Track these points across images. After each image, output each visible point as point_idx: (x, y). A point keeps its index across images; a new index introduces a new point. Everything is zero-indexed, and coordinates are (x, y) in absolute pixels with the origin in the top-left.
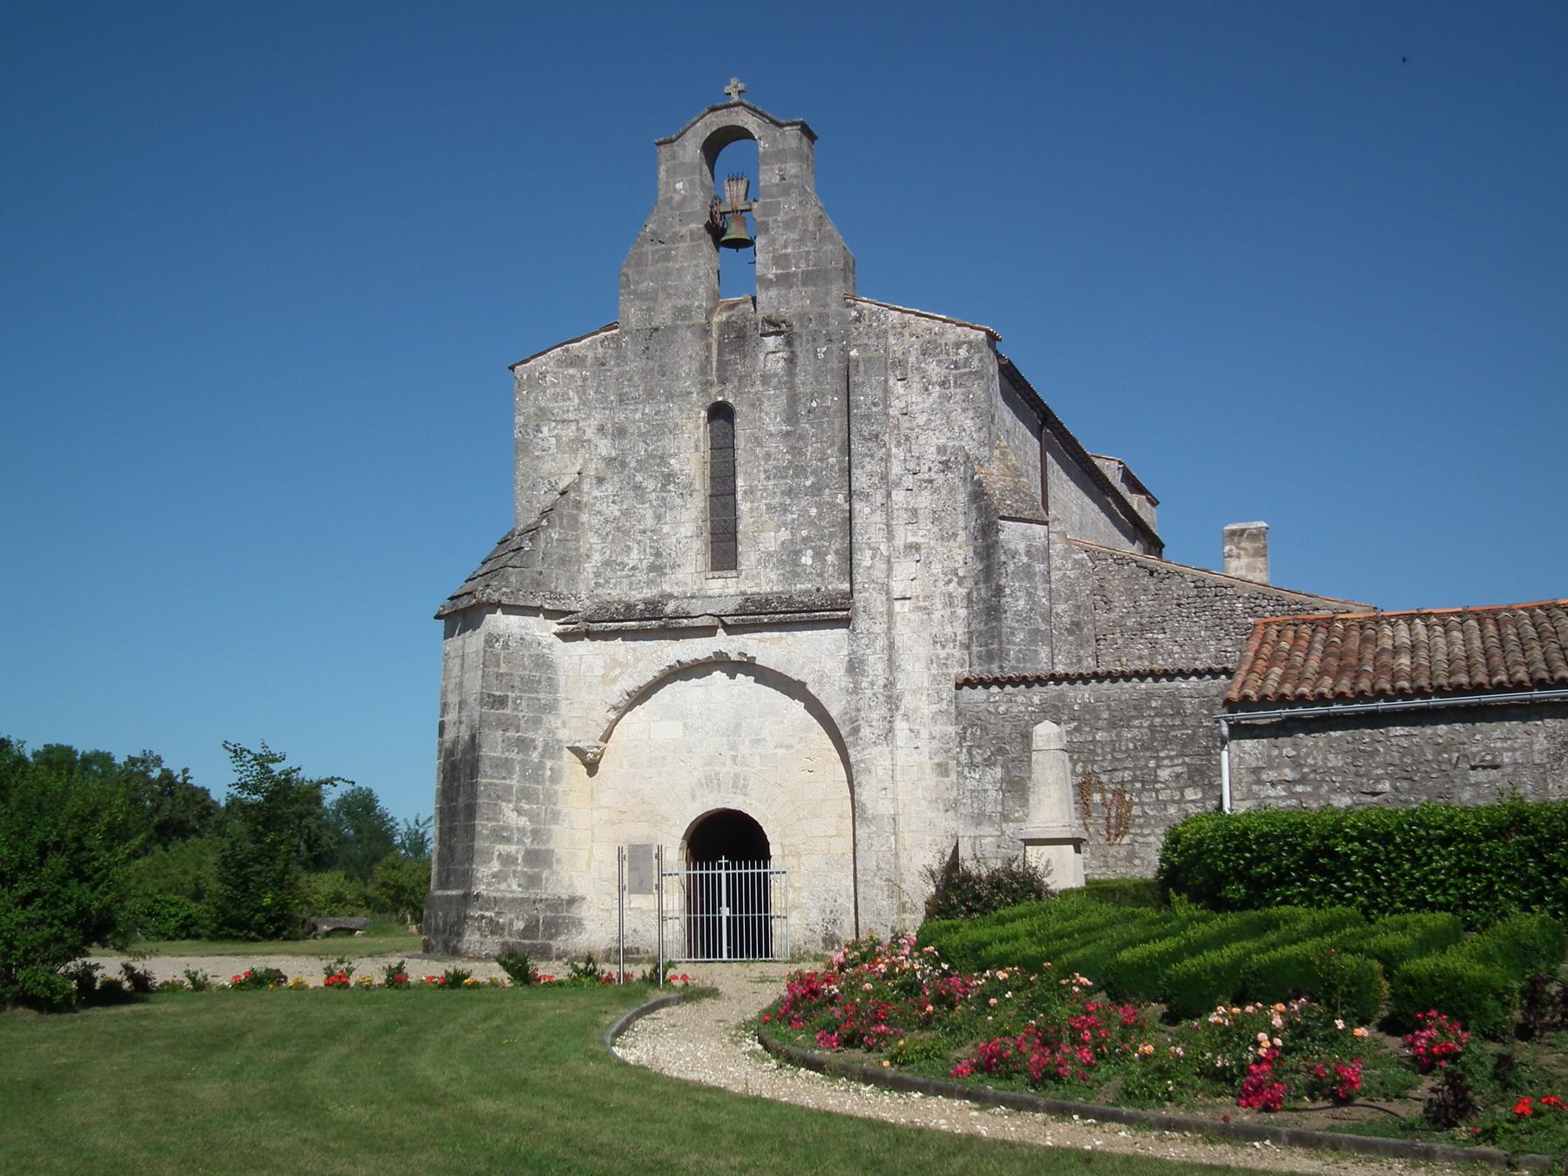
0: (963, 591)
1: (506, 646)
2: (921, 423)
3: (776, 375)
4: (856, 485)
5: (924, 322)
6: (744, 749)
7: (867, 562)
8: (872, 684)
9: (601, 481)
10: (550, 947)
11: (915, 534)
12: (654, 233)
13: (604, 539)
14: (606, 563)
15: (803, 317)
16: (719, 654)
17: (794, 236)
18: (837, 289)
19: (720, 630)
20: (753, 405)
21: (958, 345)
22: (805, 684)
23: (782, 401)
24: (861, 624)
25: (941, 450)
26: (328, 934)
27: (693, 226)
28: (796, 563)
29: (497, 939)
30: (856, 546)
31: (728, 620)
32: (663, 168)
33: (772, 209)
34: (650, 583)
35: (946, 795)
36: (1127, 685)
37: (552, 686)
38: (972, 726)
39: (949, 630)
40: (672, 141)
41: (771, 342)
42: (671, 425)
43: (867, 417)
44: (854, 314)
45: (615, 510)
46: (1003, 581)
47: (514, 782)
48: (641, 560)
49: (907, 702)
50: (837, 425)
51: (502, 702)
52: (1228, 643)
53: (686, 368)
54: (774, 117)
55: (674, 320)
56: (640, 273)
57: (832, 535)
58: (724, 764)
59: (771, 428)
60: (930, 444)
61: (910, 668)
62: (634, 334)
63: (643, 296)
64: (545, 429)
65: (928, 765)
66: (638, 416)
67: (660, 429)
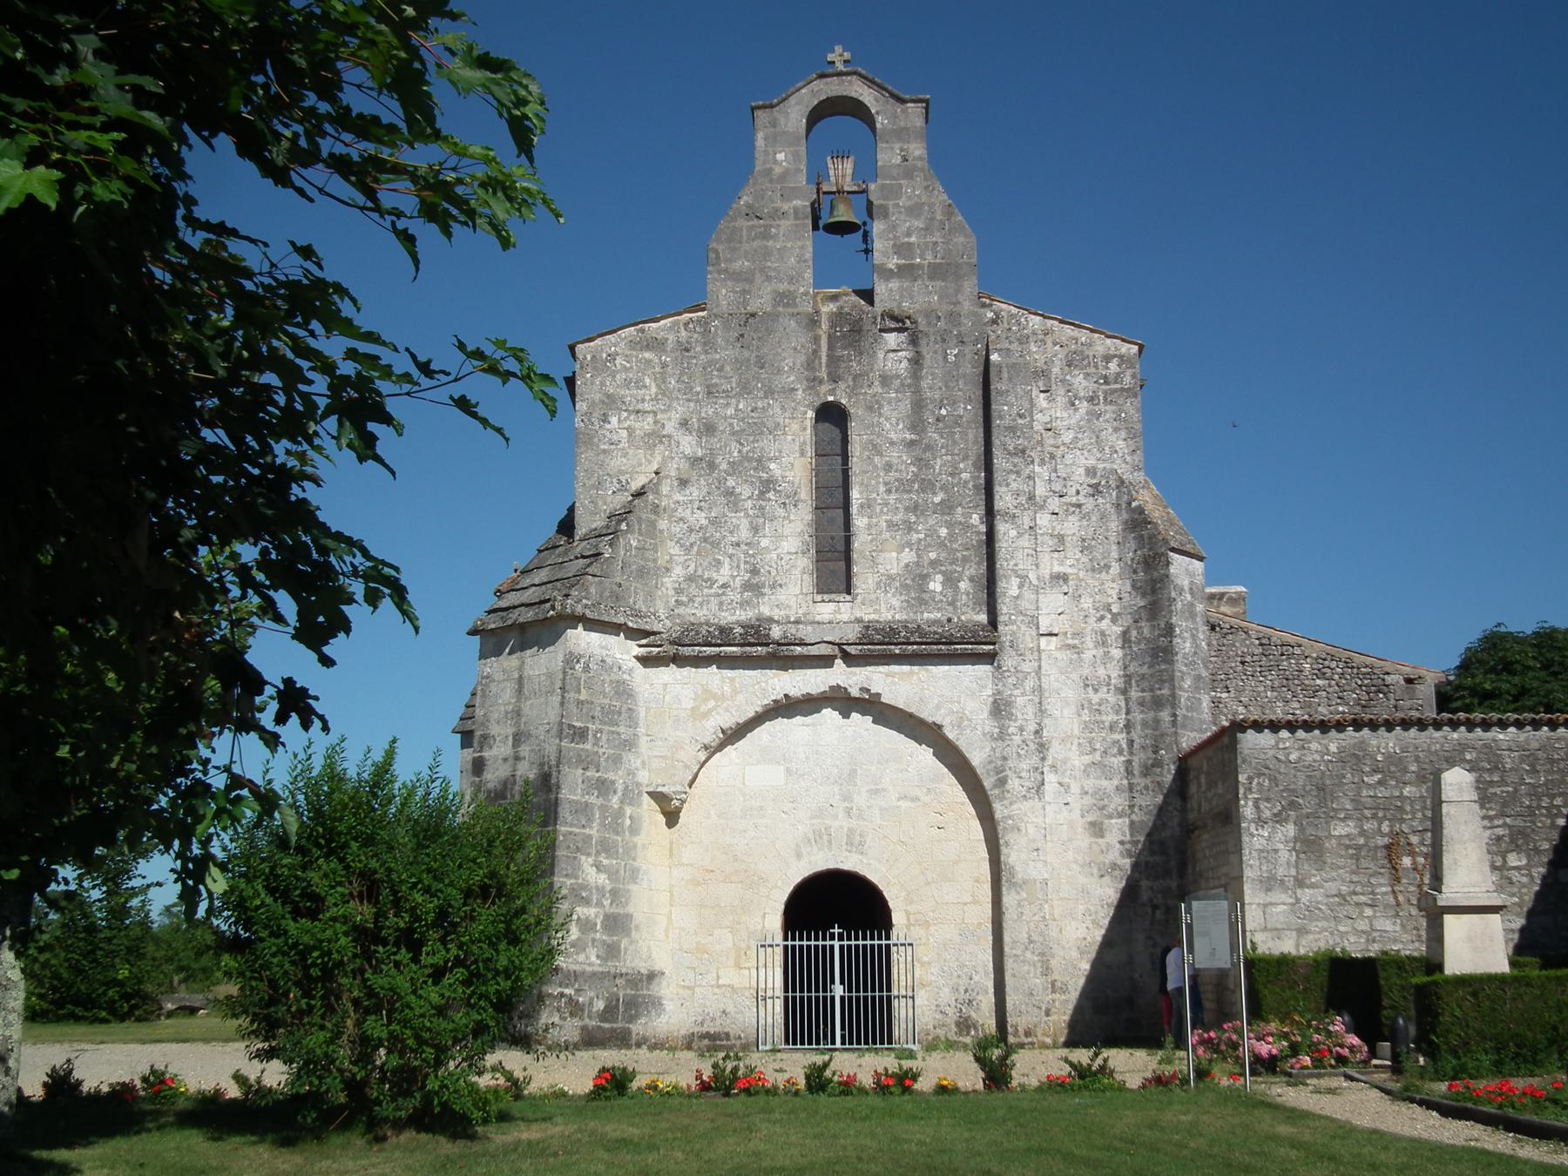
0: (1118, 629)
1: (587, 668)
2: (1067, 441)
3: (898, 376)
4: (999, 505)
5: (1068, 330)
6: (861, 800)
7: (1014, 591)
8: (1021, 729)
9: (683, 483)
10: (629, 1032)
11: (1062, 563)
12: (749, 206)
13: (688, 550)
14: (690, 579)
15: (930, 314)
16: (837, 688)
17: (919, 223)
18: (970, 286)
19: (838, 661)
20: (870, 408)
21: (1107, 359)
22: (940, 727)
23: (906, 406)
24: (1008, 660)
25: (1090, 472)
26: (170, 1014)
27: (797, 203)
28: (922, 589)
29: (576, 1022)
30: (1000, 572)
31: (852, 650)
32: (760, 136)
33: (896, 192)
34: (744, 604)
35: (1101, 858)
36: (1437, 734)
37: (633, 722)
38: (1259, 775)
40: (772, 106)
41: (892, 339)
42: (770, 424)
43: (1012, 429)
44: (990, 315)
45: (701, 518)
46: (1174, 620)
47: (593, 832)
48: (734, 578)
49: (1055, 752)
50: (971, 437)
51: (581, 735)
52: (1296, 705)
53: (789, 361)
54: (896, 92)
55: (774, 306)
56: (734, 250)
57: (965, 560)
58: (836, 817)
59: (893, 436)
60: (1078, 465)
61: (1057, 713)
62: (726, 319)
63: (737, 277)
64: (614, 420)
65: (1080, 824)
66: (730, 411)
67: (757, 428)
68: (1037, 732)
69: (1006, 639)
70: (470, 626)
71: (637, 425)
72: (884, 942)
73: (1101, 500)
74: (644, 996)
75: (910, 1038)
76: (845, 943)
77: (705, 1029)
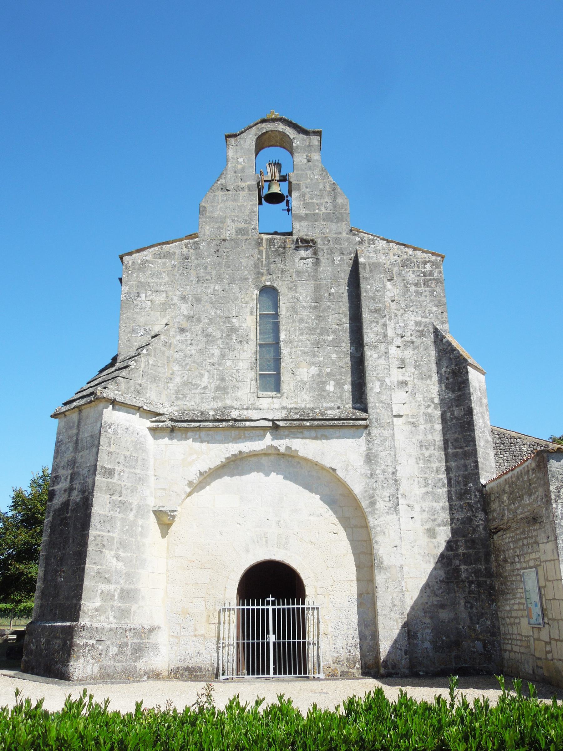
1: (115, 432)
4: (366, 339)
7: (377, 389)
14: (185, 384)
21: (425, 263)
24: (375, 431)
25: (417, 324)
31: (281, 424)
34: (215, 399)
39: (430, 437)
43: (373, 299)
44: (358, 239)
47: (115, 535)
49: (404, 487)
53: (244, 264)
64: (143, 296)
68: (393, 473)
69: (373, 417)
70: (52, 413)
71: (156, 298)
72: (301, 606)
73: (424, 339)
74: (146, 643)
75: (316, 671)
76: (276, 607)
77: (186, 665)
